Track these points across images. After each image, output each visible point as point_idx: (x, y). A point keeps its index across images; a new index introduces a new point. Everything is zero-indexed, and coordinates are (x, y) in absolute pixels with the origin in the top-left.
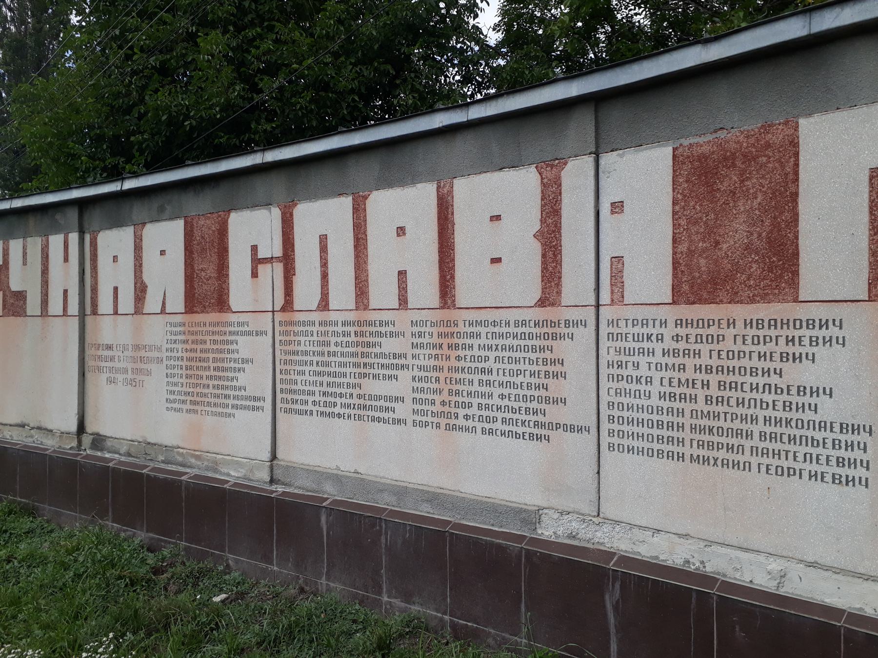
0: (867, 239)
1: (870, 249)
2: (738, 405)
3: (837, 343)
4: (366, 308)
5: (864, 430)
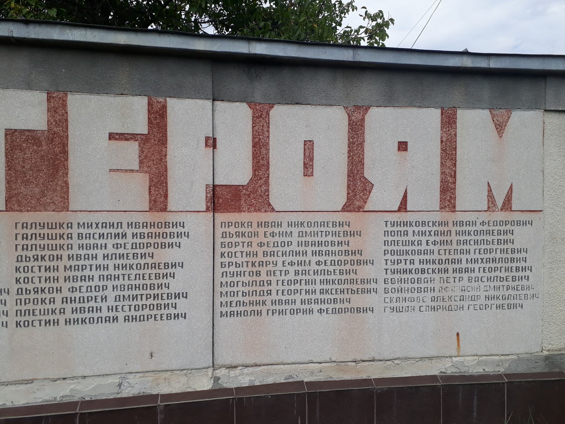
0: (4, 173)
1: (6, 178)
2: (314, 274)
3: (357, 234)
4: (164, 209)
5: (5, 292)
